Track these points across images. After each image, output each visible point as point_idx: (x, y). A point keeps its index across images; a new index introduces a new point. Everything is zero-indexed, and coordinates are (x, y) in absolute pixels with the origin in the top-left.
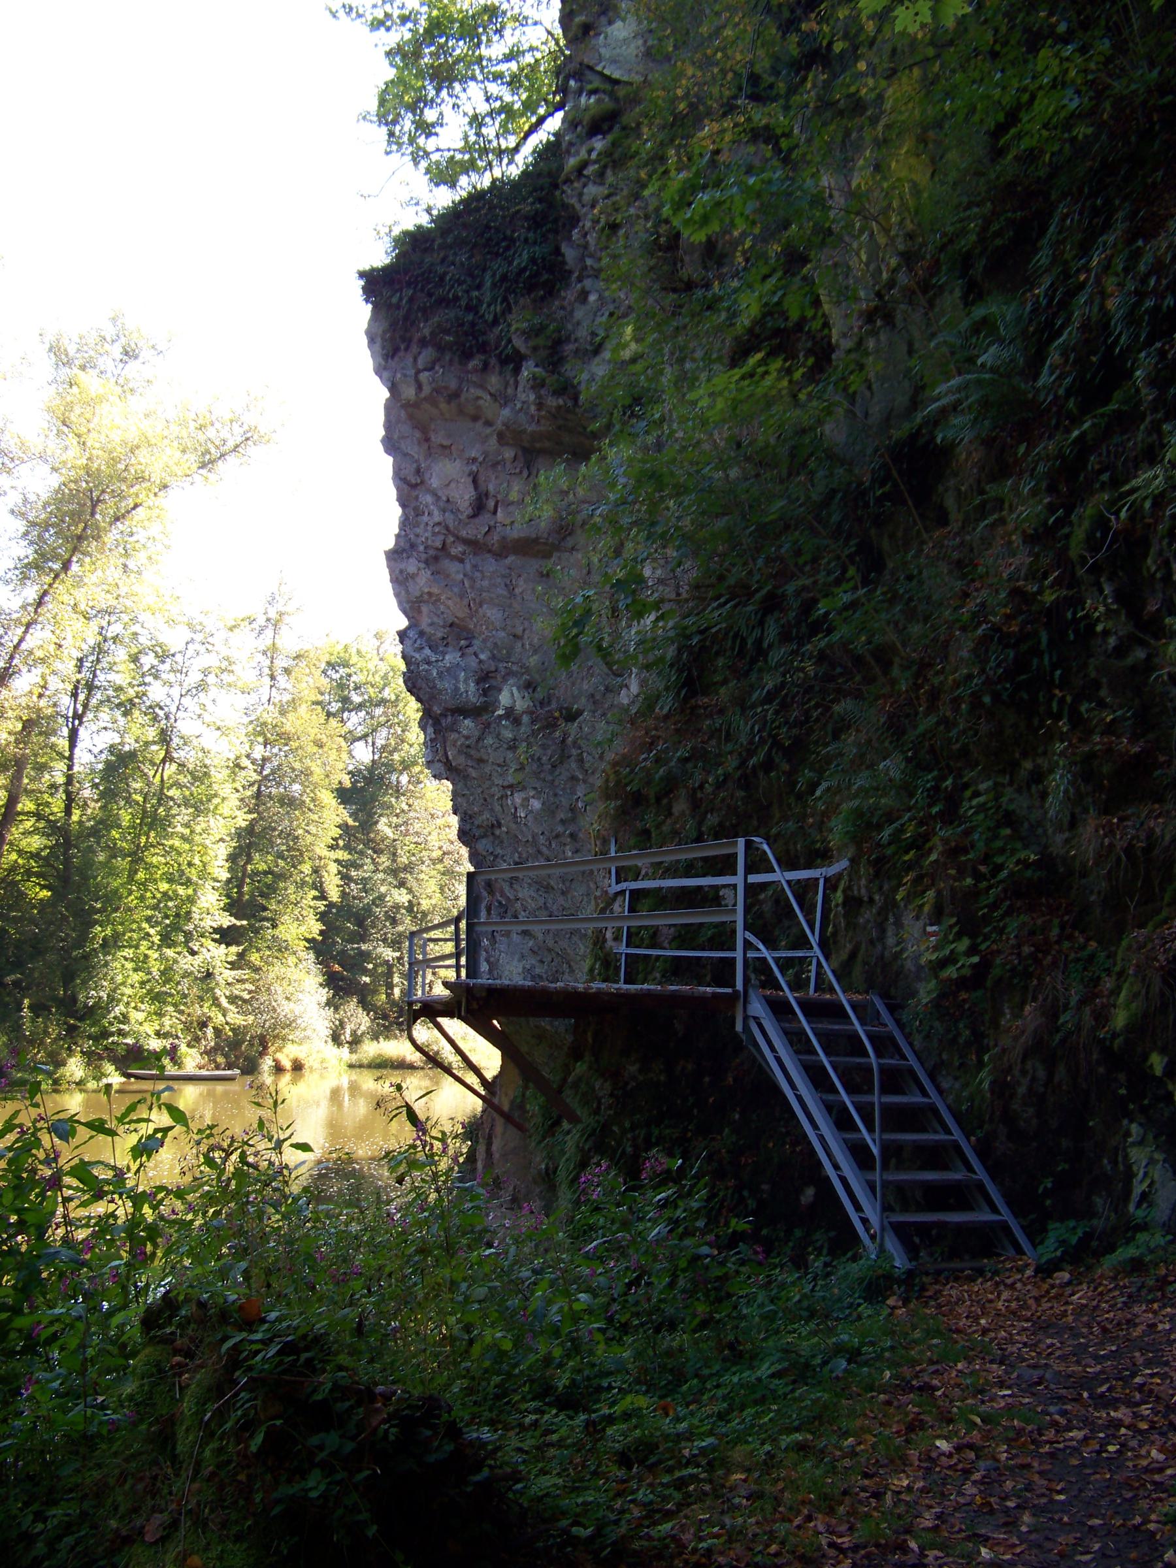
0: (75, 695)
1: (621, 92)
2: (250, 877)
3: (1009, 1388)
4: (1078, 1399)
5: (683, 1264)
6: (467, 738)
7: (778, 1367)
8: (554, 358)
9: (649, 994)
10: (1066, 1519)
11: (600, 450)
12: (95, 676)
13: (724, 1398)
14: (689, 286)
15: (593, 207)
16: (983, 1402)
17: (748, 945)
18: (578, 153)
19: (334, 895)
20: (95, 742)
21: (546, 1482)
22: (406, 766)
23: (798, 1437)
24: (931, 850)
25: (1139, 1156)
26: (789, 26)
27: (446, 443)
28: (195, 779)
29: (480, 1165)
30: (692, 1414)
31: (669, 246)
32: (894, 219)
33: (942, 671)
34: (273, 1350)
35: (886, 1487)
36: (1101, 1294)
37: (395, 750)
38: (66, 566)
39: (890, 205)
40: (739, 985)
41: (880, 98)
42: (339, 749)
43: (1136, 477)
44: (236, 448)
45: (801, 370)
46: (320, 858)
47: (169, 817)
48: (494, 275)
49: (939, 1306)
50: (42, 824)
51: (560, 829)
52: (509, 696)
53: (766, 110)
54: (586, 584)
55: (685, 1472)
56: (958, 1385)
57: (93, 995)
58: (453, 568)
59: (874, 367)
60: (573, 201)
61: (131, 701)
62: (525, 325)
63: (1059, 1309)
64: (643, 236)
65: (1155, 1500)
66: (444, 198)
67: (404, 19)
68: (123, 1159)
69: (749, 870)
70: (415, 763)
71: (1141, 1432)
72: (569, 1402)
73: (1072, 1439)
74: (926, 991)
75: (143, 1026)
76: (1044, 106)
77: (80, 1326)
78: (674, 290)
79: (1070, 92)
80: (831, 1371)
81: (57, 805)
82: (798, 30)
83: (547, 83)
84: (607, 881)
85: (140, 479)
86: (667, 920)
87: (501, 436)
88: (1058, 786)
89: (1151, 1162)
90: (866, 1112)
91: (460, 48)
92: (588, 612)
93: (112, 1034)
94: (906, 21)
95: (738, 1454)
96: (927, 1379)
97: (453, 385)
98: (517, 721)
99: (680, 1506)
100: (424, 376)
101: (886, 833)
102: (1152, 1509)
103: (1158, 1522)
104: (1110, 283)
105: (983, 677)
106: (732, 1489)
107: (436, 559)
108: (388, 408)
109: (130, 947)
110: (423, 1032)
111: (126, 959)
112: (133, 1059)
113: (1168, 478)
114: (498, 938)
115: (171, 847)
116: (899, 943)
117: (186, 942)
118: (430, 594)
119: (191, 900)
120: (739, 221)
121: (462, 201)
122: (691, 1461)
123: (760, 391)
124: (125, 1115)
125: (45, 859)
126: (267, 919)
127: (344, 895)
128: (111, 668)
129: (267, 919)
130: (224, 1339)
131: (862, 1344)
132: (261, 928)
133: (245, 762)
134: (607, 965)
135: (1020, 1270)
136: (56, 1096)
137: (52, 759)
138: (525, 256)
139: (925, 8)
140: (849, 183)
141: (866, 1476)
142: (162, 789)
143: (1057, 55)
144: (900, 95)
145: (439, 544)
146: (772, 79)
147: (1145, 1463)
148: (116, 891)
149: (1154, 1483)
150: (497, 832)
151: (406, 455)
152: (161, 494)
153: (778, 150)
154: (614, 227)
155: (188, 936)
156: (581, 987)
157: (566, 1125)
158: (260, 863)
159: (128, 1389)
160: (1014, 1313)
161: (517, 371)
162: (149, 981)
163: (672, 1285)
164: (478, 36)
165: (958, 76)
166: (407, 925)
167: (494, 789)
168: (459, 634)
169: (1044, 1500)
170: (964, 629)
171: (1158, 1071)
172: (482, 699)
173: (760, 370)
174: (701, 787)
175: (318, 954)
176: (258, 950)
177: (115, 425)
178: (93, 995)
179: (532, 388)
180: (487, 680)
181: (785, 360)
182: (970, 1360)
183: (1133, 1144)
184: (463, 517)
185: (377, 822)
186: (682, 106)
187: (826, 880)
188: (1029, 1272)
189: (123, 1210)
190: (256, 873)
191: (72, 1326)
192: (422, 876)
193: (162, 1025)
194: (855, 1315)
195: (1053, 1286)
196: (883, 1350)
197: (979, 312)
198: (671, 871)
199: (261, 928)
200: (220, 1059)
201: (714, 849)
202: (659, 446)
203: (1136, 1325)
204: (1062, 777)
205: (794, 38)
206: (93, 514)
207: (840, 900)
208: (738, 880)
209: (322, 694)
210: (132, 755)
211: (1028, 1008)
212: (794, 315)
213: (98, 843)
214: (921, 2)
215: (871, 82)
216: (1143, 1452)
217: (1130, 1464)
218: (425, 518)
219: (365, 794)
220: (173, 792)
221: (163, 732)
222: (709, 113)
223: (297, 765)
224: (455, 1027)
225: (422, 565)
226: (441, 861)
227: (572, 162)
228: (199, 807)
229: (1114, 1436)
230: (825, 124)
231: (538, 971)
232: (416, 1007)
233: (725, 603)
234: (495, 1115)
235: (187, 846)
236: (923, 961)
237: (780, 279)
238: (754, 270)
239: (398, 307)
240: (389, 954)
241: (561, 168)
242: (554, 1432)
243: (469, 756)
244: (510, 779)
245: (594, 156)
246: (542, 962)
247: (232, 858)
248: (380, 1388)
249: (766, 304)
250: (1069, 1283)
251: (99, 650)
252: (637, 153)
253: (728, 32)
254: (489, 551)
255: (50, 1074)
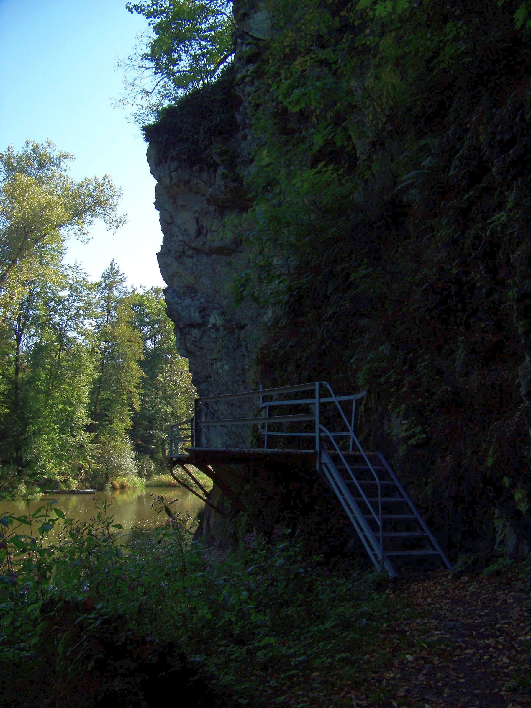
0: (19, 321)
1: (261, 44)
2: (100, 401)
3: (440, 630)
4: (471, 635)
5: (292, 576)
6: (195, 338)
7: (334, 623)
8: (232, 165)
9: (276, 454)
10: (464, 690)
11: (252, 206)
12: (28, 312)
13: (311, 637)
14: (292, 132)
15: (249, 96)
16: (428, 637)
17: (321, 430)
18: (242, 72)
19: (138, 409)
20: (28, 341)
21: (229, 678)
22: (170, 350)
23: (343, 655)
24: (403, 386)
25: (499, 523)
26: (335, 13)
27: (183, 204)
28: (74, 357)
29: (204, 531)
30: (296, 645)
31: (282, 114)
32: (384, 100)
33: (407, 305)
34: (99, 622)
35: (384, 678)
36: (482, 587)
37: (165, 343)
38: (14, 262)
39: (382, 94)
40: (317, 449)
41: (377, 45)
42: (139, 343)
43: (494, 216)
44: (90, 208)
45: (342, 170)
46: (131, 392)
47: (63, 375)
48: (204, 128)
49: (409, 593)
50: (5, 379)
51: (238, 378)
52: (214, 319)
53: (325, 52)
54: (247, 267)
55: (291, 673)
56: (417, 630)
57: (28, 456)
58: (188, 261)
59: (376, 168)
60: (240, 94)
61: (44, 323)
62: (219, 150)
63: (463, 593)
64: (271, 109)
65: (504, 681)
66: (181, 93)
67: (162, 12)
68: (36, 534)
69: (321, 396)
70: (174, 349)
71: (500, 650)
72: (240, 642)
73: (468, 654)
74: (402, 450)
75: (53, 470)
76: (449, 49)
77: (12, 613)
78: (285, 134)
79: (461, 42)
80: (359, 624)
81: (12, 370)
82: (339, 15)
83: (228, 42)
84: (258, 402)
85: (47, 222)
86: (286, 420)
87: (208, 200)
88: (460, 357)
89: (504, 526)
90: (375, 505)
91: (189, 25)
92: (247, 280)
93: (38, 474)
94: (382, 11)
95: (316, 663)
96: (402, 627)
97: (187, 177)
98: (217, 330)
99: (289, 688)
100: (173, 174)
101: (383, 379)
102: (503, 686)
103: (506, 691)
104: (481, 128)
105: (426, 307)
106: (313, 679)
107: (180, 257)
108: (157, 188)
109: (46, 434)
110: (178, 471)
111: (44, 439)
112: (48, 485)
113: (508, 217)
114: (210, 428)
115: (64, 388)
116: (389, 429)
117: (71, 432)
118: (178, 273)
119: (74, 412)
120: (313, 102)
121: (190, 94)
122: (296, 667)
123: (323, 179)
124: (36, 514)
125: (7, 395)
126: (108, 421)
127: (142, 409)
128: (35, 309)
129: (108, 421)
130: (78, 617)
131: (373, 612)
132: (105, 424)
133: (97, 350)
134: (259, 440)
135: (446, 576)
136: (13, 502)
137: (9, 350)
138: (218, 119)
139: (389, 5)
140: (363, 84)
141: (375, 672)
142: (59, 363)
143: (455, 26)
144: (387, 45)
145: (181, 250)
146: (328, 38)
147: (500, 664)
148: (39, 410)
149: (504, 673)
150: (209, 380)
151: (166, 210)
152: (57, 229)
153: (330, 70)
154: (258, 106)
155: (72, 428)
156: (246, 450)
157: (242, 513)
158: (104, 395)
159: (34, 641)
160: (443, 596)
161: (215, 171)
162: (54, 449)
163: (287, 586)
164: (196, 20)
165: (412, 36)
166: (171, 422)
167: (207, 361)
168: (191, 290)
169: (454, 682)
170: (417, 286)
171: (507, 485)
172: (202, 320)
173: (324, 170)
174: (300, 359)
175: (131, 435)
176: (104, 434)
177: (37, 196)
178: (28, 456)
179: (222, 178)
180: (203, 311)
181: (335, 165)
182: (422, 618)
183: (497, 518)
184: (192, 237)
185: (157, 376)
186: (287, 50)
187: (357, 400)
188: (450, 577)
189: (35, 557)
190: (103, 400)
191: (8, 613)
192: (178, 400)
193: (61, 469)
194: (371, 598)
195: (460, 583)
196: (383, 614)
197: (423, 142)
198: (288, 397)
199: (105, 424)
200: (88, 484)
201: (306, 387)
202: (280, 205)
203: (498, 600)
204: (462, 352)
205: (337, 19)
206: (26, 238)
207: (363, 409)
208: (316, 401)
209: (131, 318)
210: (45, 347)
211: (448, 458)
212: (339, 144)
213: (30, 387)
214: (387, 2)
215: (371, 38)
216: (500, 659)
217: (494, 664)
218: (175, 238)
219: (151, 363)
220: (64, 364)
221: (59, 337)
222: (300, 53)
223: (120, 351)
224: (192, 468)
225: (174, 260)
226: (186, 393)
227: (239, 76)
228: (77, 370)
229: (487, 652)
230: (352, 58)
231: (229, 443)
232: (175, 459)
233: (309, 275)
234: (211, 508)
235: (71, 388)
236: (400, 437)
237: (332, 128)
238: (321, 125)
239: (161, 142)
240: (164, 435)
241: (234, 79)
242: (232, 654)
243: (196, 346)
244: (215, 356)
245: (249, 73)
246: (230, 438)
247: (91, 393)
248: (149, 639)
249: (326, 140)
250: (468, 581)
251: (30, 300)
252: (268, 71)
253: (307, 17)
254: (204, 253)
255: (10, 492)
